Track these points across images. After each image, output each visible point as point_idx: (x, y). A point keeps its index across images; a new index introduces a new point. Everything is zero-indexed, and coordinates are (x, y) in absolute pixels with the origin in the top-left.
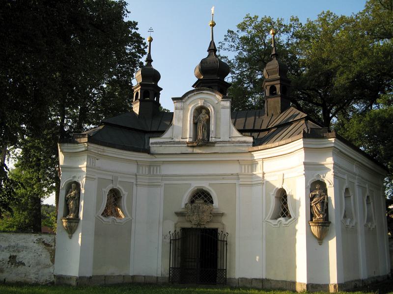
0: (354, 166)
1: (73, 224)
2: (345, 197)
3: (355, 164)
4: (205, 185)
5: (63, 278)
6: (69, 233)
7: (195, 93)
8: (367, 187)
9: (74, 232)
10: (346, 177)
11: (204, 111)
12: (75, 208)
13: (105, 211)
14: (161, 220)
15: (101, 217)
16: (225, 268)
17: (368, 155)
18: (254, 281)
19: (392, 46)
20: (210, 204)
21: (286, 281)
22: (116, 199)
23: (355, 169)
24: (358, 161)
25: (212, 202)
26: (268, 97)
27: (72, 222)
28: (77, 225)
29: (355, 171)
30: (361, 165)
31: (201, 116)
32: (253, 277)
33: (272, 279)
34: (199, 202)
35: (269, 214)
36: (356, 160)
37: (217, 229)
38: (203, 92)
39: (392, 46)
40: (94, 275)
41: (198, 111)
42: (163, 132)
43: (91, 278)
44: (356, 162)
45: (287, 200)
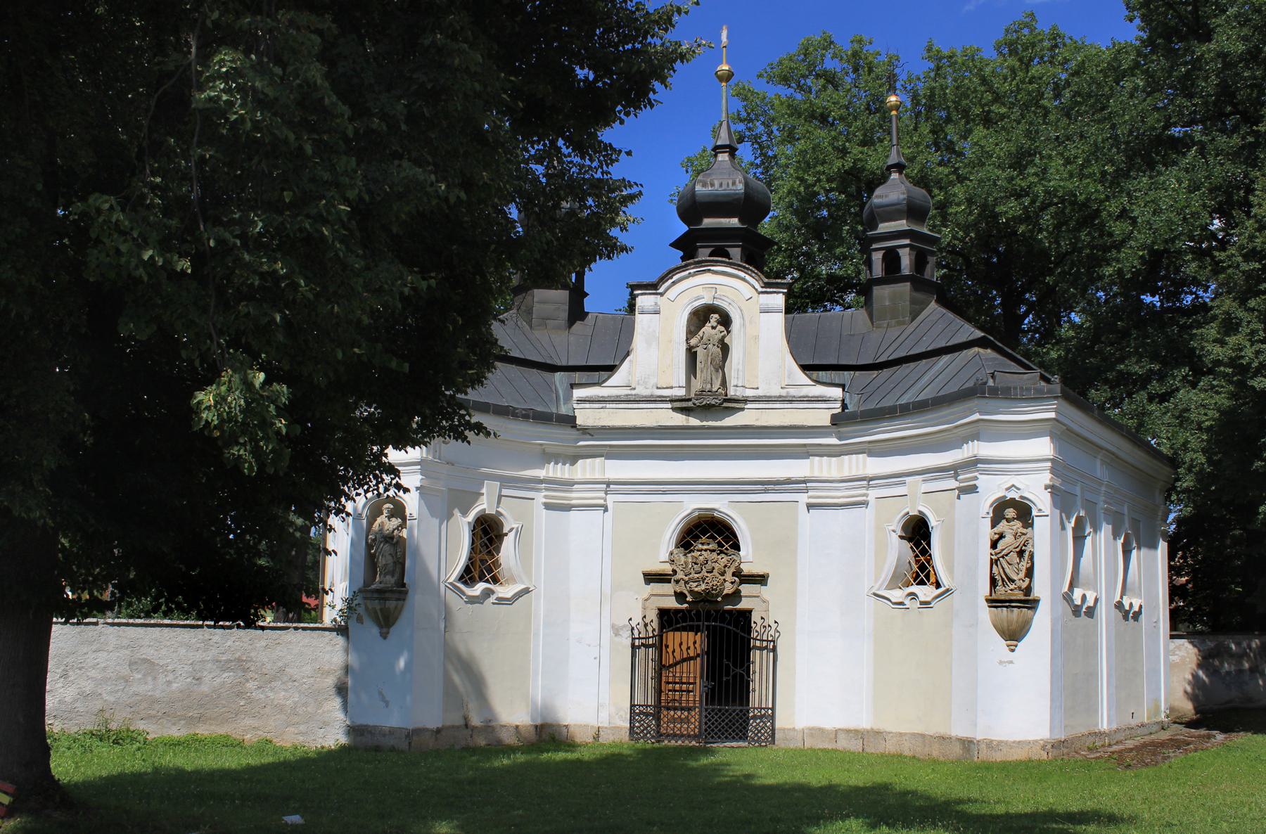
0: (1098, 462)
1: (391, 604)
2: (1074, 538)
3: (1099, 457)
4: (720, 505)
5: (370, 732)
6: (380, 626)
7: (692, 271)
8: (1126, 512)
9: (393, 624)
10: (1078, 491)
11: (714, 317)
12: (394, 563)
13: (467, 570)
14: (607, 589)
15: (460, 585)
16: (770, 706)
17: (1117, 422)
18: (841, 736)
19: (1264, 217)
20: (731, 551)
21: (923, 736)
22: (491, 540)
23: (1100, 470)
24: (1107, 450)
25: (737, 547)
26: (879, 282)
27: (386, 599)
28: (403, 606)
29: (1099, 474)
30: (1113, 459)
31: (707, 329)
32: (838, 727)
33: (888, 730)
34: (705, 549)
35: (883, 576)
36: (1102, 448)
37: (750, 612)
38: (712, 268)
39: (1264, 217)
40: (448, 723)
41: (698, 318)
42: (611, 369)
43: (438, 731)
44: (1104, 452)
45: (929, 544)
